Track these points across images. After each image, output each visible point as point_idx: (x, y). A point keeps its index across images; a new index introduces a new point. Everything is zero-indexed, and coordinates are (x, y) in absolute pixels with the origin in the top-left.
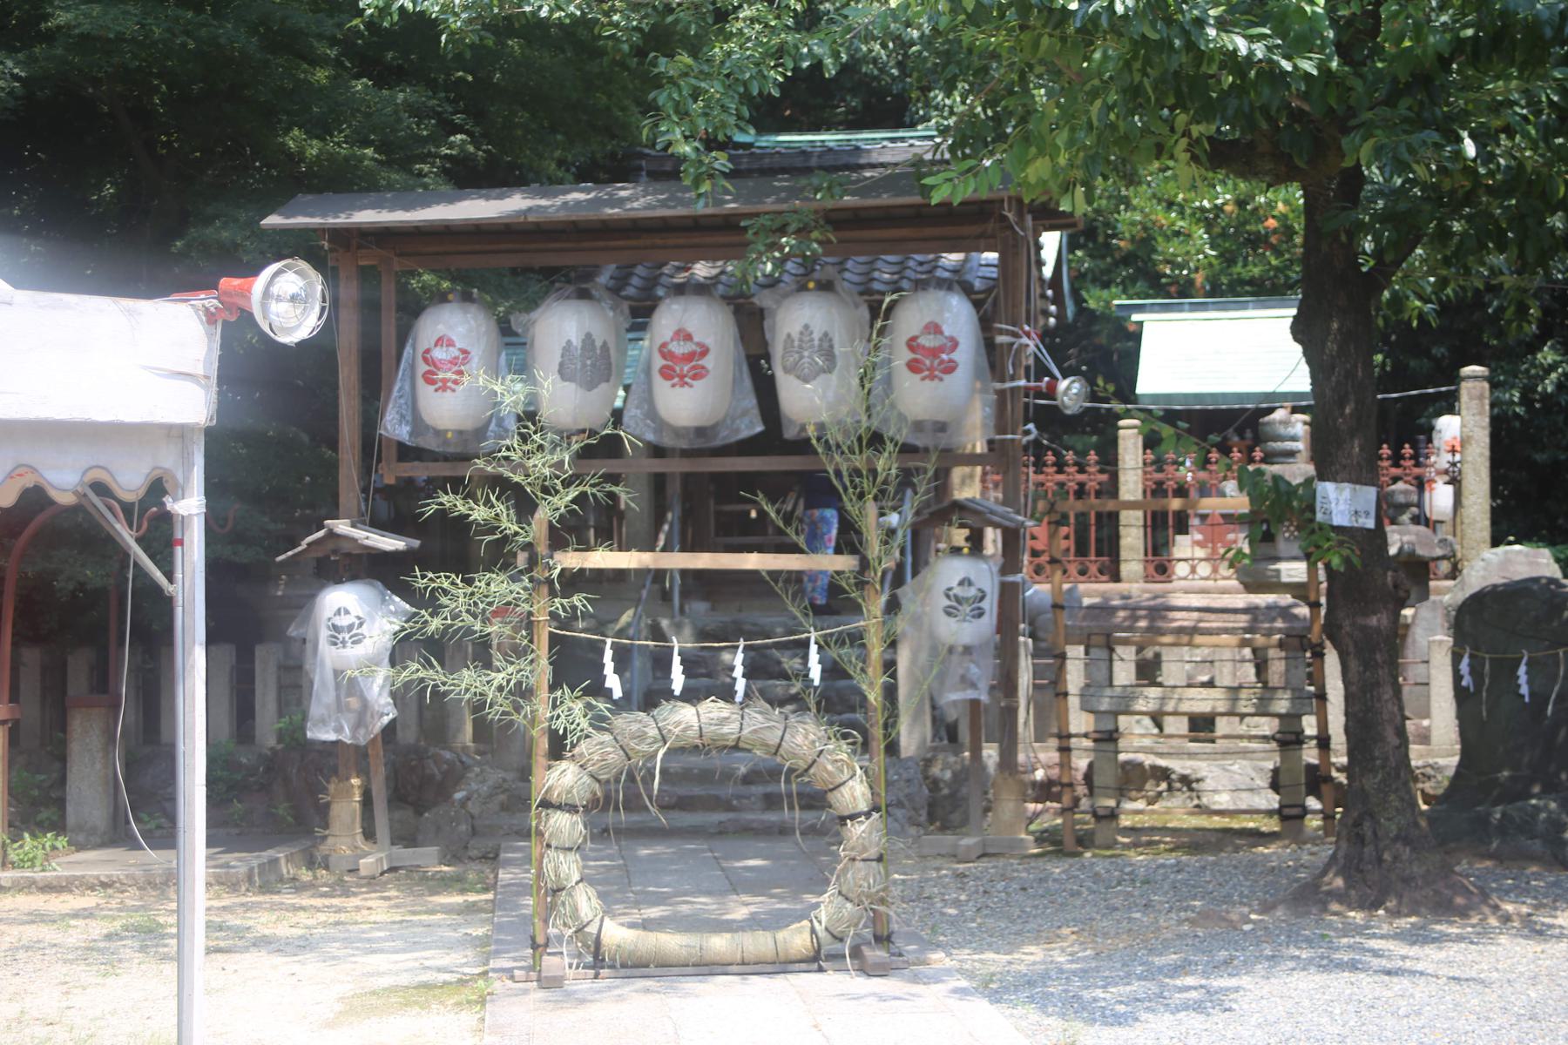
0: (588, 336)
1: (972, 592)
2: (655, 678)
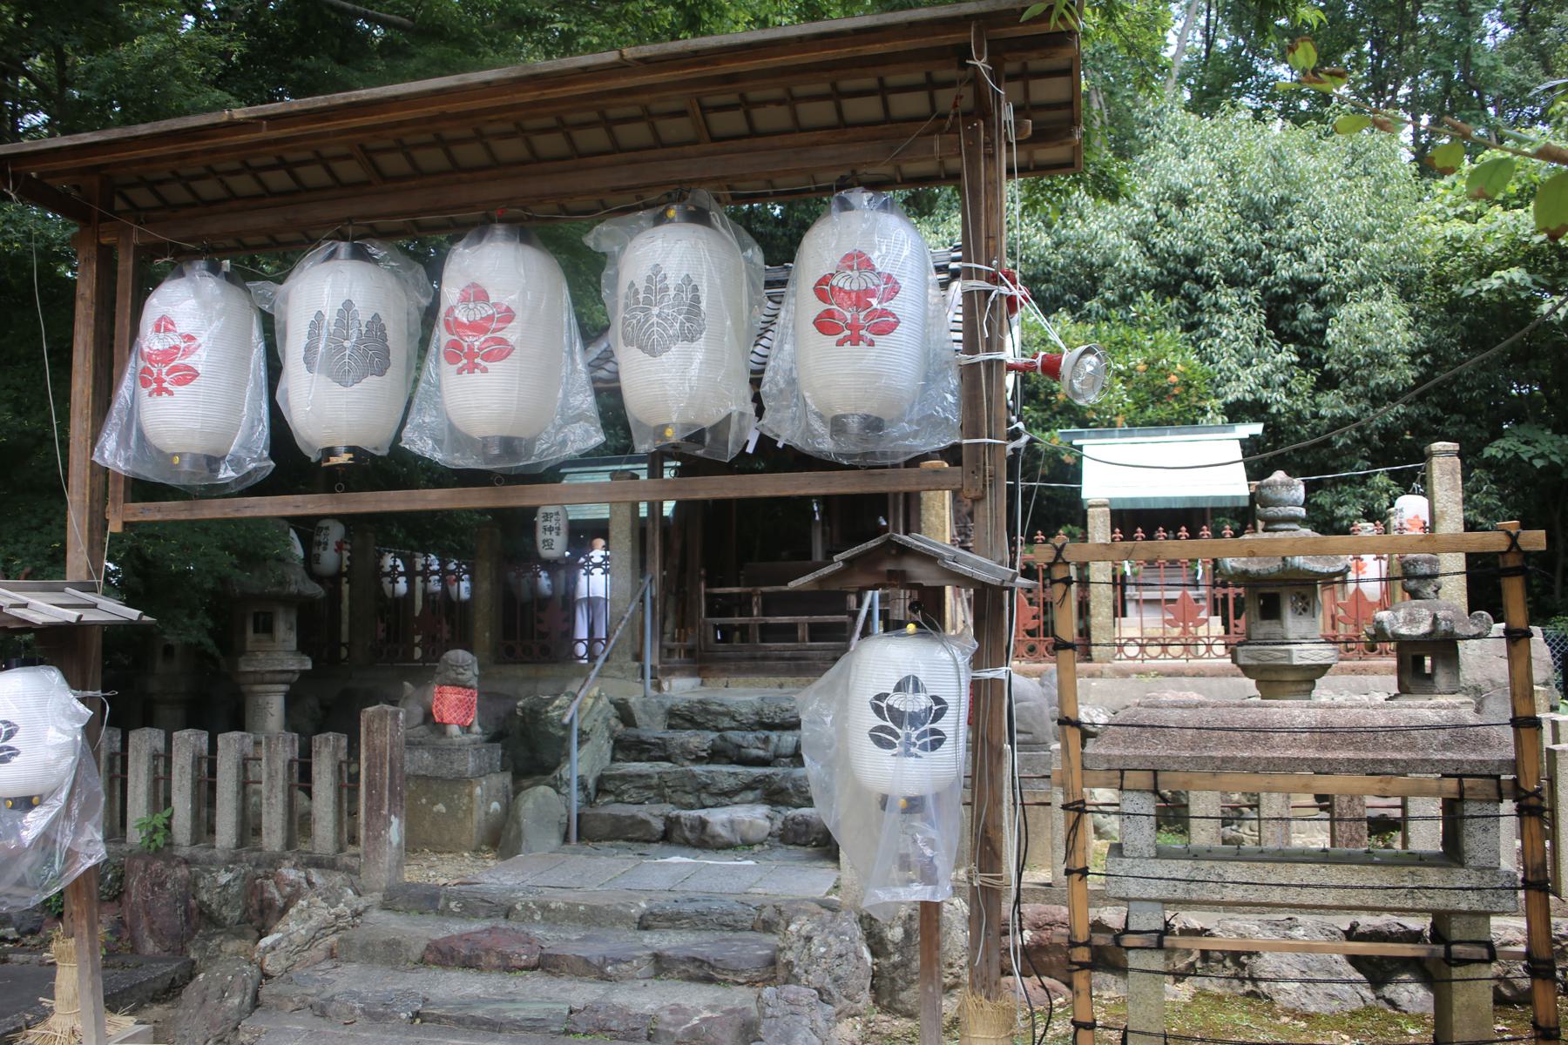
0: (348, 304)
1: (922, 702)
2: (614, 759)
